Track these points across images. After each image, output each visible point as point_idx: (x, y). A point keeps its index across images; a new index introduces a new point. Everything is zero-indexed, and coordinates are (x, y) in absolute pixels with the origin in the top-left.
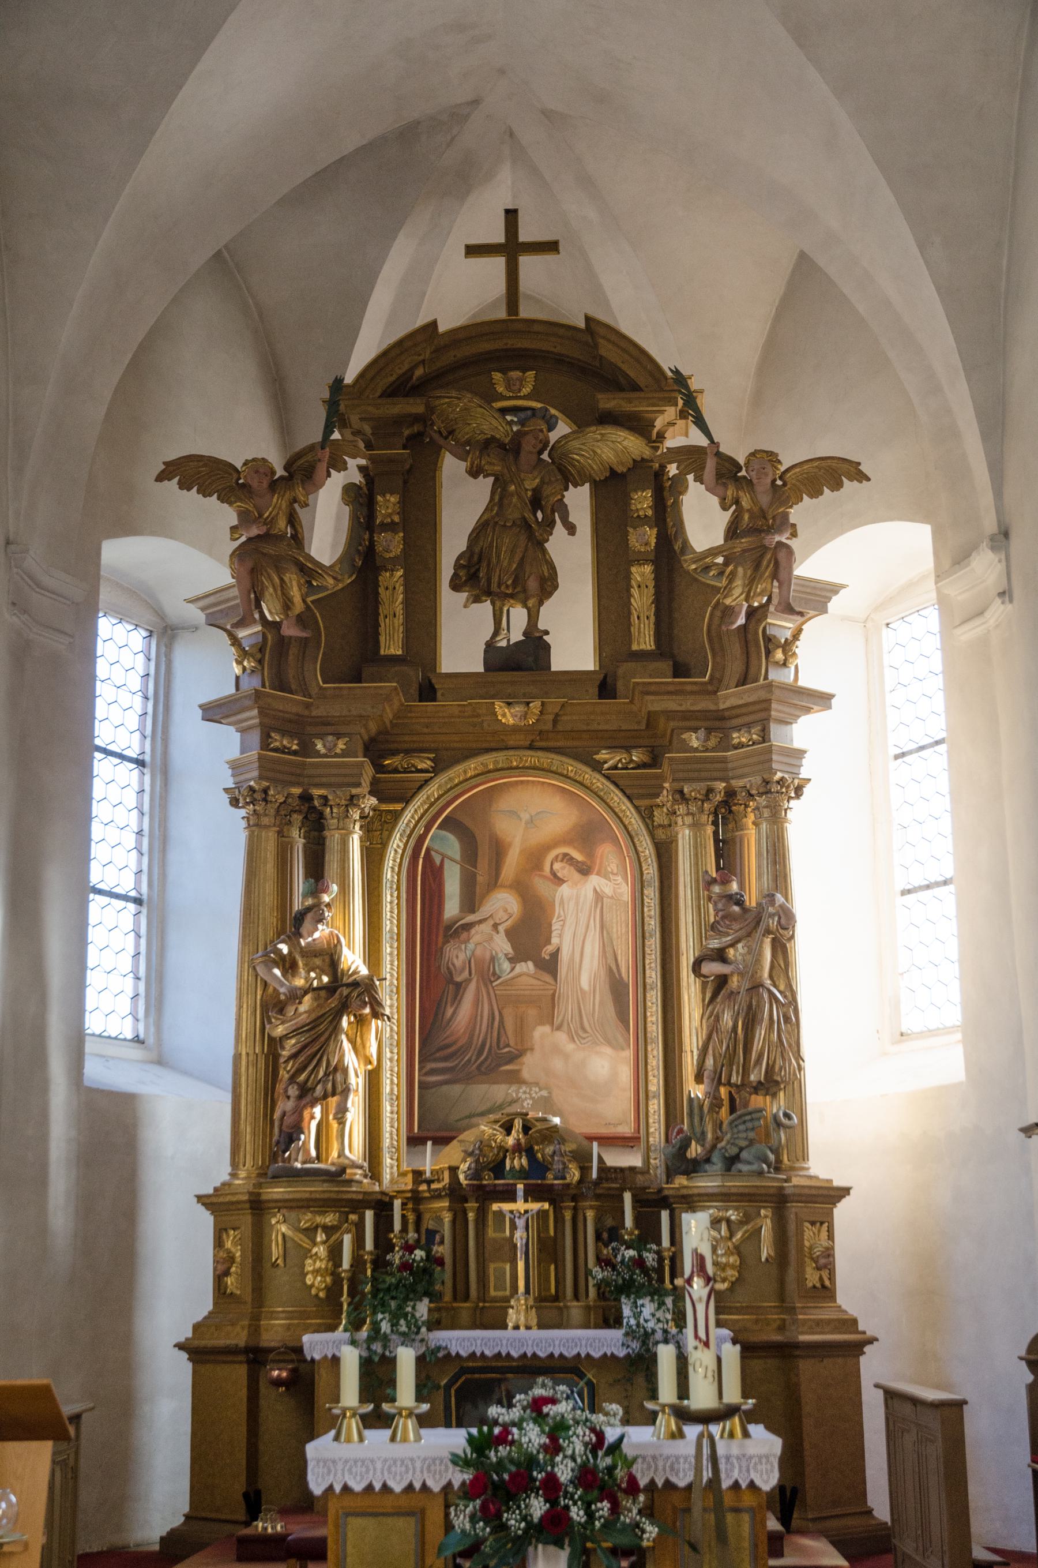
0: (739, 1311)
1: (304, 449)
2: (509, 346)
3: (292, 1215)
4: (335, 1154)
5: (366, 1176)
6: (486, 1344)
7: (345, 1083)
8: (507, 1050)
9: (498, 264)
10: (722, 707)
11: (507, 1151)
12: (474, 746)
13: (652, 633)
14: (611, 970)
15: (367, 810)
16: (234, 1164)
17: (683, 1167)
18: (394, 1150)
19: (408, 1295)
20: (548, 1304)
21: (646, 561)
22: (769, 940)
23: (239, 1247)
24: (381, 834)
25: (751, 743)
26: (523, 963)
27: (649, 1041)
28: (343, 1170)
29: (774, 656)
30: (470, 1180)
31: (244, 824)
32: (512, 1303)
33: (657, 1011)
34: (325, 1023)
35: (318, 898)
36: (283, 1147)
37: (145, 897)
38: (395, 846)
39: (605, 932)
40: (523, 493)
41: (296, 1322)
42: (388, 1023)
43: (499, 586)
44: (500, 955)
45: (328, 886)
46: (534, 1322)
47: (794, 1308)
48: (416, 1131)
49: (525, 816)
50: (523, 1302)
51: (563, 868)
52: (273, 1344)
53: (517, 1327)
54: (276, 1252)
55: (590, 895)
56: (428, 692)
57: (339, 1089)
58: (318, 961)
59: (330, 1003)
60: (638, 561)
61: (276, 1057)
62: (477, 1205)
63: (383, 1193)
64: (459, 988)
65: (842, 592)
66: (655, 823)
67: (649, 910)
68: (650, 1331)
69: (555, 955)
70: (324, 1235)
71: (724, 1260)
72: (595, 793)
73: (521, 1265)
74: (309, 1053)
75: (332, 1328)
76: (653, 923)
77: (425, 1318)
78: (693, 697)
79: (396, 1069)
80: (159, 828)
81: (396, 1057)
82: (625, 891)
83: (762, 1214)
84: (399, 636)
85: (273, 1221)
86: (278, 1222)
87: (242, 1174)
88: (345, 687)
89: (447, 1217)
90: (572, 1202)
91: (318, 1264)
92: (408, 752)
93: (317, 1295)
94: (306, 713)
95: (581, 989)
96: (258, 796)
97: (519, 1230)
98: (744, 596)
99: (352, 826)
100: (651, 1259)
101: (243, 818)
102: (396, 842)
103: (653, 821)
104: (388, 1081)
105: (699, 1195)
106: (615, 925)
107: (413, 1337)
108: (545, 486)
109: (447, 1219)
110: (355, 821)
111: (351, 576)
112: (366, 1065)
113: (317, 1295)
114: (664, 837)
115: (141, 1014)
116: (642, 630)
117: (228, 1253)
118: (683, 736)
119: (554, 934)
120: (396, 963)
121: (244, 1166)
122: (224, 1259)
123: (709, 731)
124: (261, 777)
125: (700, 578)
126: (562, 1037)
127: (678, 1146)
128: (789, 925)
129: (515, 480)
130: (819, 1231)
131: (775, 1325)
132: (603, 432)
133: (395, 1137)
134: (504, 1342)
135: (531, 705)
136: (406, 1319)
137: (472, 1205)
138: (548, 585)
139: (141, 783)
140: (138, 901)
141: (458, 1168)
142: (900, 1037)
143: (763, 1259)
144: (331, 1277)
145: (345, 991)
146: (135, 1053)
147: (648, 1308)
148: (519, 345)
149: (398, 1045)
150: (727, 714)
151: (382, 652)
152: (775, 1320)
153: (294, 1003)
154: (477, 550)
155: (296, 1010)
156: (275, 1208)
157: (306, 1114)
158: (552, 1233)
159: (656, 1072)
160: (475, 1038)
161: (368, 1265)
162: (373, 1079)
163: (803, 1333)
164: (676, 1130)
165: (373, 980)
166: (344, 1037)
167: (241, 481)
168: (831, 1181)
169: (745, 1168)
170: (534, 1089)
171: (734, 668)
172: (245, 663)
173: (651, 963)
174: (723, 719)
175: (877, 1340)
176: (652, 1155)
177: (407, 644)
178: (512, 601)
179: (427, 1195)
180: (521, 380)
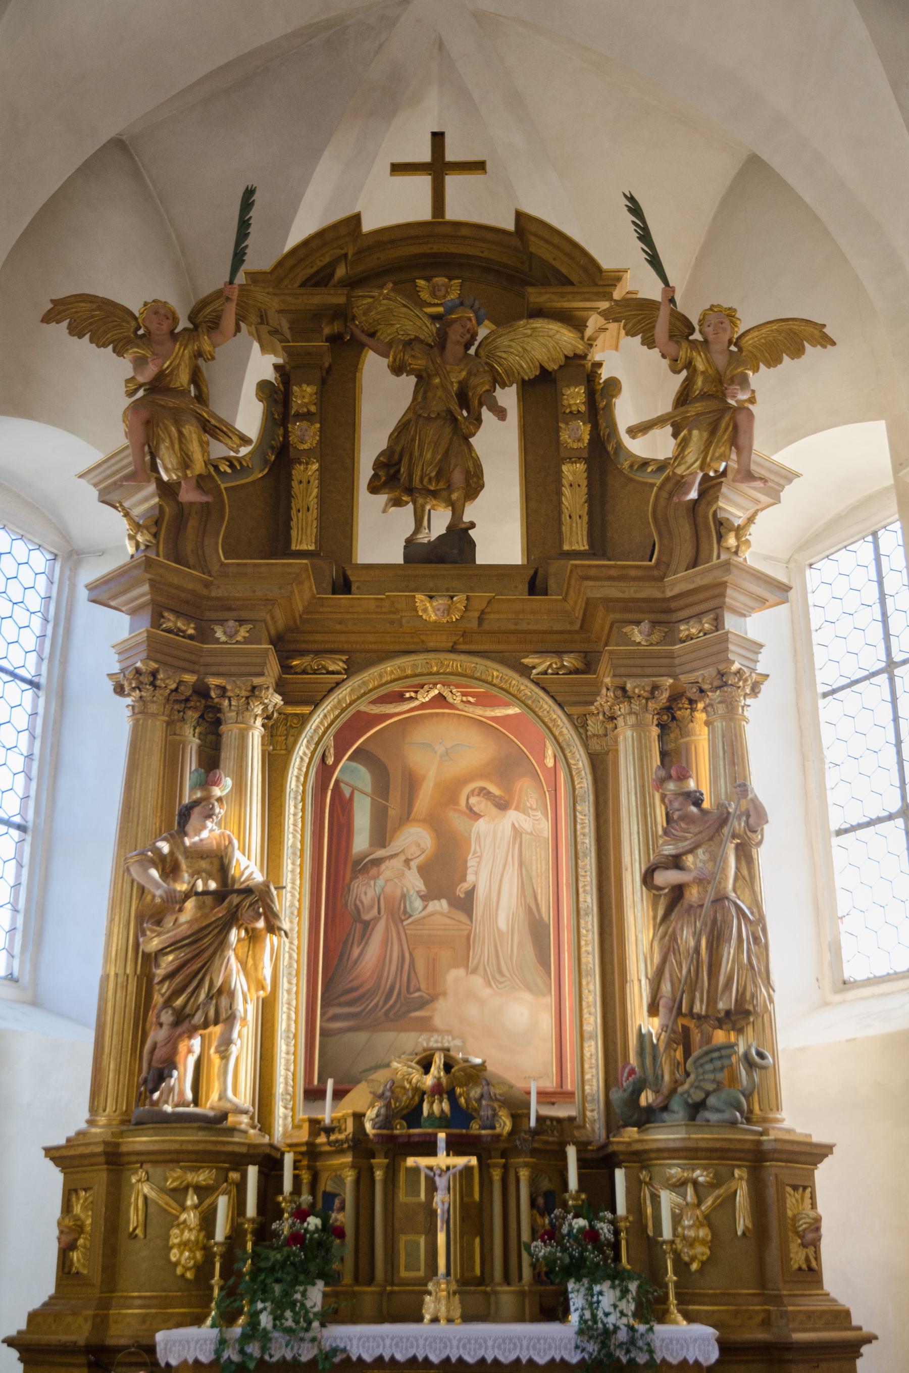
0: (713, 1299)
1: (210, 295)
2: (435, 251)
3: (157, 1172)
4: (214, 1097)
5: (254, 1127)
6: (397, 1345)
7: (231, 1008)
8: (417, 994)
9: (424, 182)
10: (669, 594)
11: (424, 1093)
12: (391, 648)
13: (585, 533)
14: (530, 911)
15: (270, 709)
16: (93, 1110)
17: (636, 1117)
18: (288, 1097)
19: (296, 1277)
20: (473, 1288)
21: (579, 459)
22: (733, 845)
23: (90, 1213)
24: (286, 739)
25: (701, 634)
26: (436, 902)
27: (583, 973)
28: (224, 1116)
29: (726, 542)
30: (379, 1128)
31: (128, 712)
32: (430, 1287)
33: (593, 939)
34: (210, 936)
36: (150, 1086)
37: (30, 824)
38: (301, 753)
39: (524, 869)
40: (449, 385)
41: (154, 1311)
42: (285, 939)
43: (421, 480)
44: (412, 892)
45: (220, 779)
46: (457, 1313)
47: (780, 1296)
48: (316, 1082)
49: (440, 749)
50: (443, 1286)
51: (479, 803)
52: (123, 1342)
53: (435, 1320)
54: (134, 1218)
55: (508, 831)
56: (343, 586)
57: (223, 1015)
58: (204, 864)
59: (217, 913)
60: (570, 459)
61: (150, 978)
62: (387, 1161)
63: (272, 1146)
64: (367, 927)
65: (796, 481)
66: (589, 733)
67: (583, 828)
68: (611, 1327)
69: (471, 893)
70: (195, 1197)
71: (691, 1233)
72: (522, 702)
73: (441, 1238)
74: (189, 971)
75: (198, 1321)
76: (587, 841)
77: (317, 1309)
78: (636, 584)
79: (294, 1003)
80: (51, 751)
81: (295, 989)
82: (545, 828)
83: (736, 1176)
85: (134, 1180)
86: (139, 1181)
87: (102, 1120)
88: (250, 564)
89: (349, 1176)
90: (502, 1158)
91: (186, 1235)
92: (318, 653)
93: (183, 1276)
94: (205, 592)
95: (498, 929)
96: (146, 679)
97: (439, 1192)
98: (698, 463)
99: (252, 721)
100: (606, 1231)
101: (128, 706)
102: (302, 749)
103: (587, 731)
104: (285, 1016)
105: (659, 1150)
106: (534, 863)
107: (302, 1335)
108: (473, 378)
109: (349, 1179)
110: (256, 716)
111: (261, 471)
112: (257, 990)
113: (183, 1276)
114: (598, 748)
115: (17, 950)
116: (574, 529)
117: (75, 1220)
118: (624, 630)
119: (470, 871)
120: (298, 882)
121: (104, 1110)
122: (70, 1228)
123: (654, 623)
124: (149, 658)
125: (636, 478)
126: (477, 981)
127: (630, 1089)
128: (759, 825)
129: (440, 372)
130: (802, 1198)
131: (758, 1319)
132: (534, 325)
133: (291, 1082)
134: (421, 1342)
135: (455, 599)
136: (293, 1311)
137: (380, 1162)
139: (35, 705)
140: (21, 828)
141: (364, 1115)
142: (842, 985)
143: (739, 1233)
144: (203, 1252)
145: (235, 899)
146: (7, 991)
147: (607, 1296)
148: (445, 250)
149: (297, 975)
150: (673, 605)
151: (293, 547)
152: (757, 1312)
153: (173, 912)
154: (398, 449)
155: (176, 920)
156: (137, 1162)
157: (182, 1047)
158: (477, 1197)
159: (593, 1010)
160: (383, 982)
161: (249, 1237)
162: (267, 1009)
163: (795, 1330)
164: (627, 1070)
165: (268, 887)
166: (231, 954)
167: (141, 332)
168: (810, 1136)
169: (713, 1117)
170: (446, 1037)
171: (684, 551)
172: (140, 538)
173: (585, 885)
174: (669, 611)
175: (876, 1338)
176: (589, 1106)
178: (434, 502)
179: (327, 1148)
180: (448, 287)
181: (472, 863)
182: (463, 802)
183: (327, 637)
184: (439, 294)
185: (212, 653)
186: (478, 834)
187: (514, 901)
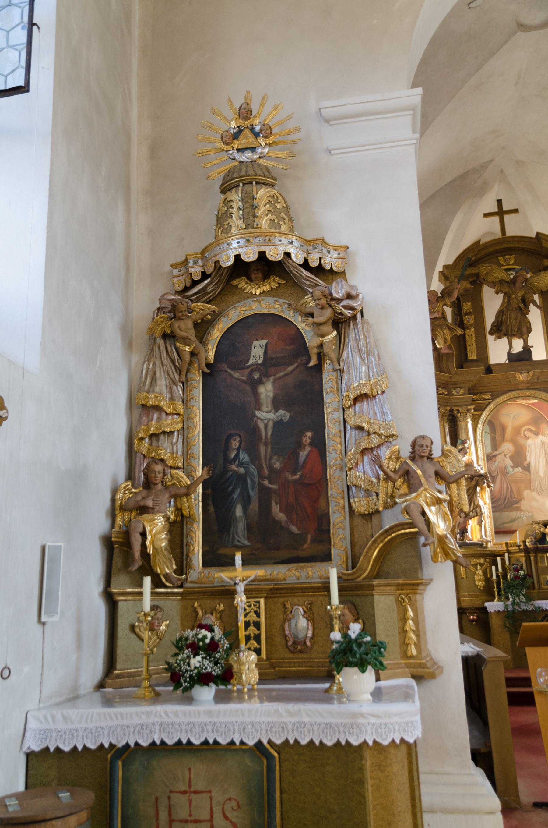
2: (505, 247)
8: (514, 499)
9: (496, 219)
12: (506, 389)
35: (464, 445)
43: (511, 332)
44: (508, 466)
49: (512, 416)
55: (540, 443)
57: (479, 514)
69: (529, 465)
84: (475, 352)
91: (479, 577)
92: (481, 393)
95: (540, 477)
119: (528, 457)
126: (534, 494)
138: (529, 330)
151: (469, 358)
177: (478, 355)
181: (528, 454)
182: (522, 434)
183: (484, 388)
184: (507, 262)
185: (453, 399)
186: (529, 444)
187: (545, 467)
